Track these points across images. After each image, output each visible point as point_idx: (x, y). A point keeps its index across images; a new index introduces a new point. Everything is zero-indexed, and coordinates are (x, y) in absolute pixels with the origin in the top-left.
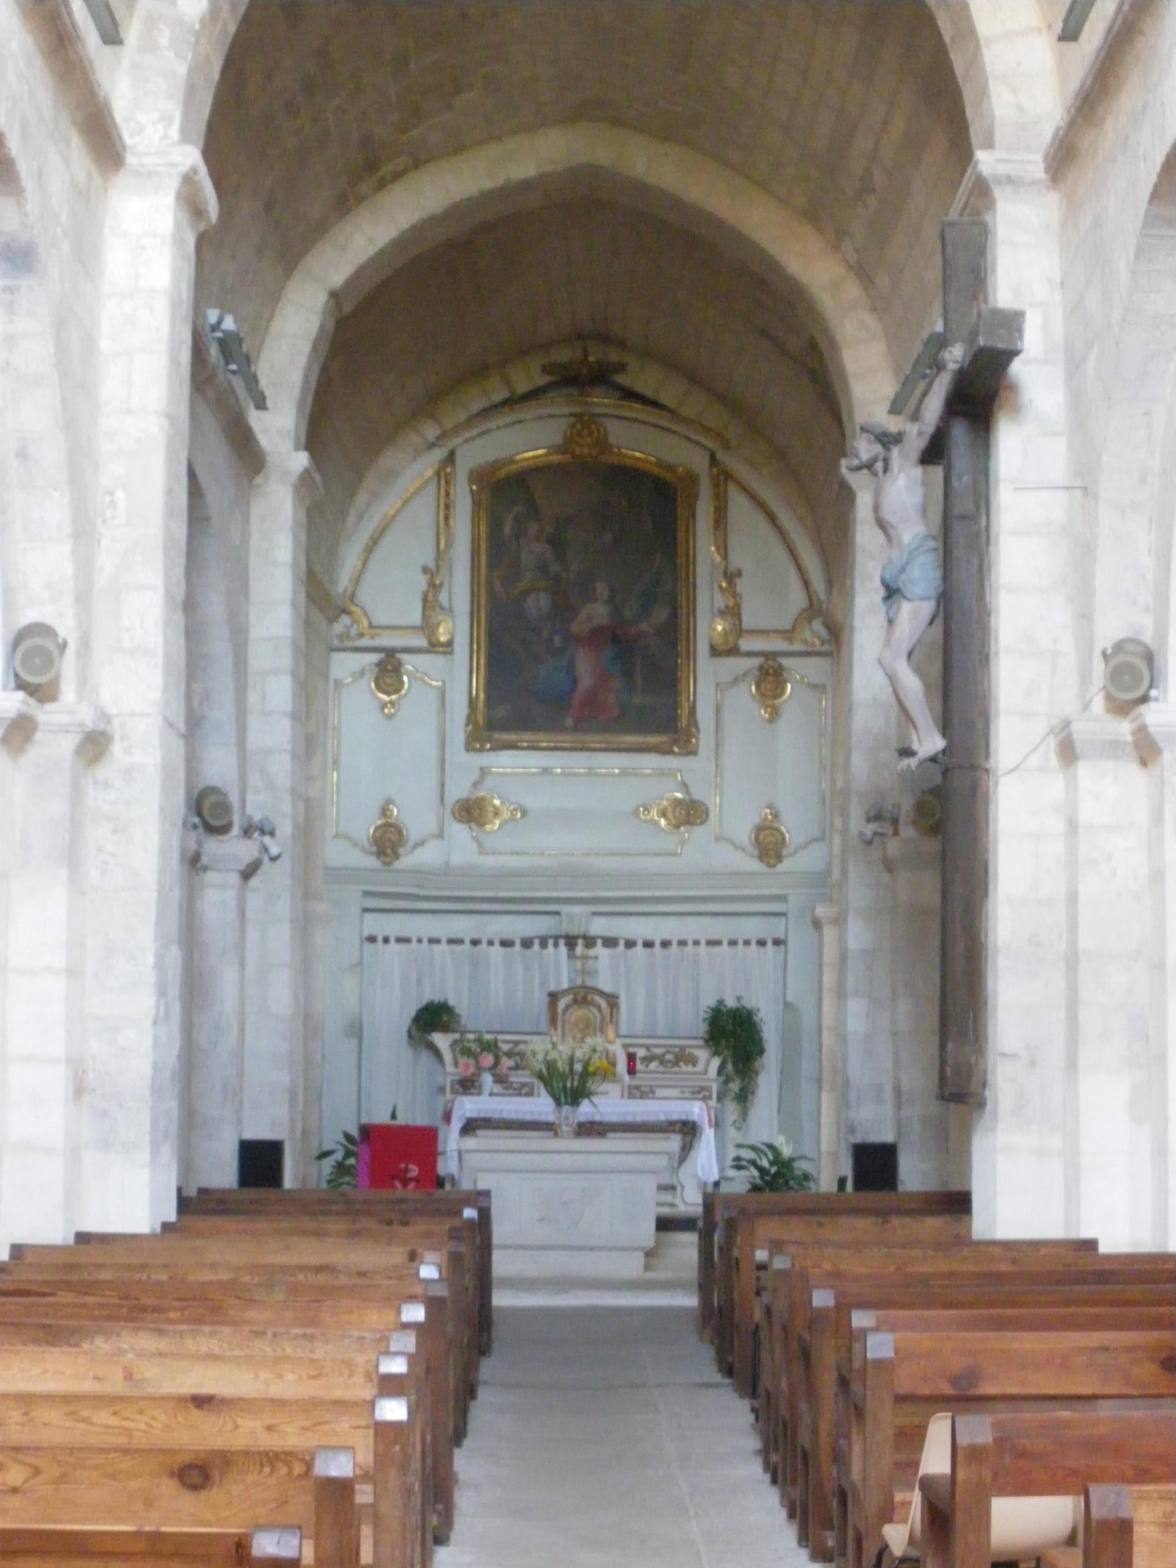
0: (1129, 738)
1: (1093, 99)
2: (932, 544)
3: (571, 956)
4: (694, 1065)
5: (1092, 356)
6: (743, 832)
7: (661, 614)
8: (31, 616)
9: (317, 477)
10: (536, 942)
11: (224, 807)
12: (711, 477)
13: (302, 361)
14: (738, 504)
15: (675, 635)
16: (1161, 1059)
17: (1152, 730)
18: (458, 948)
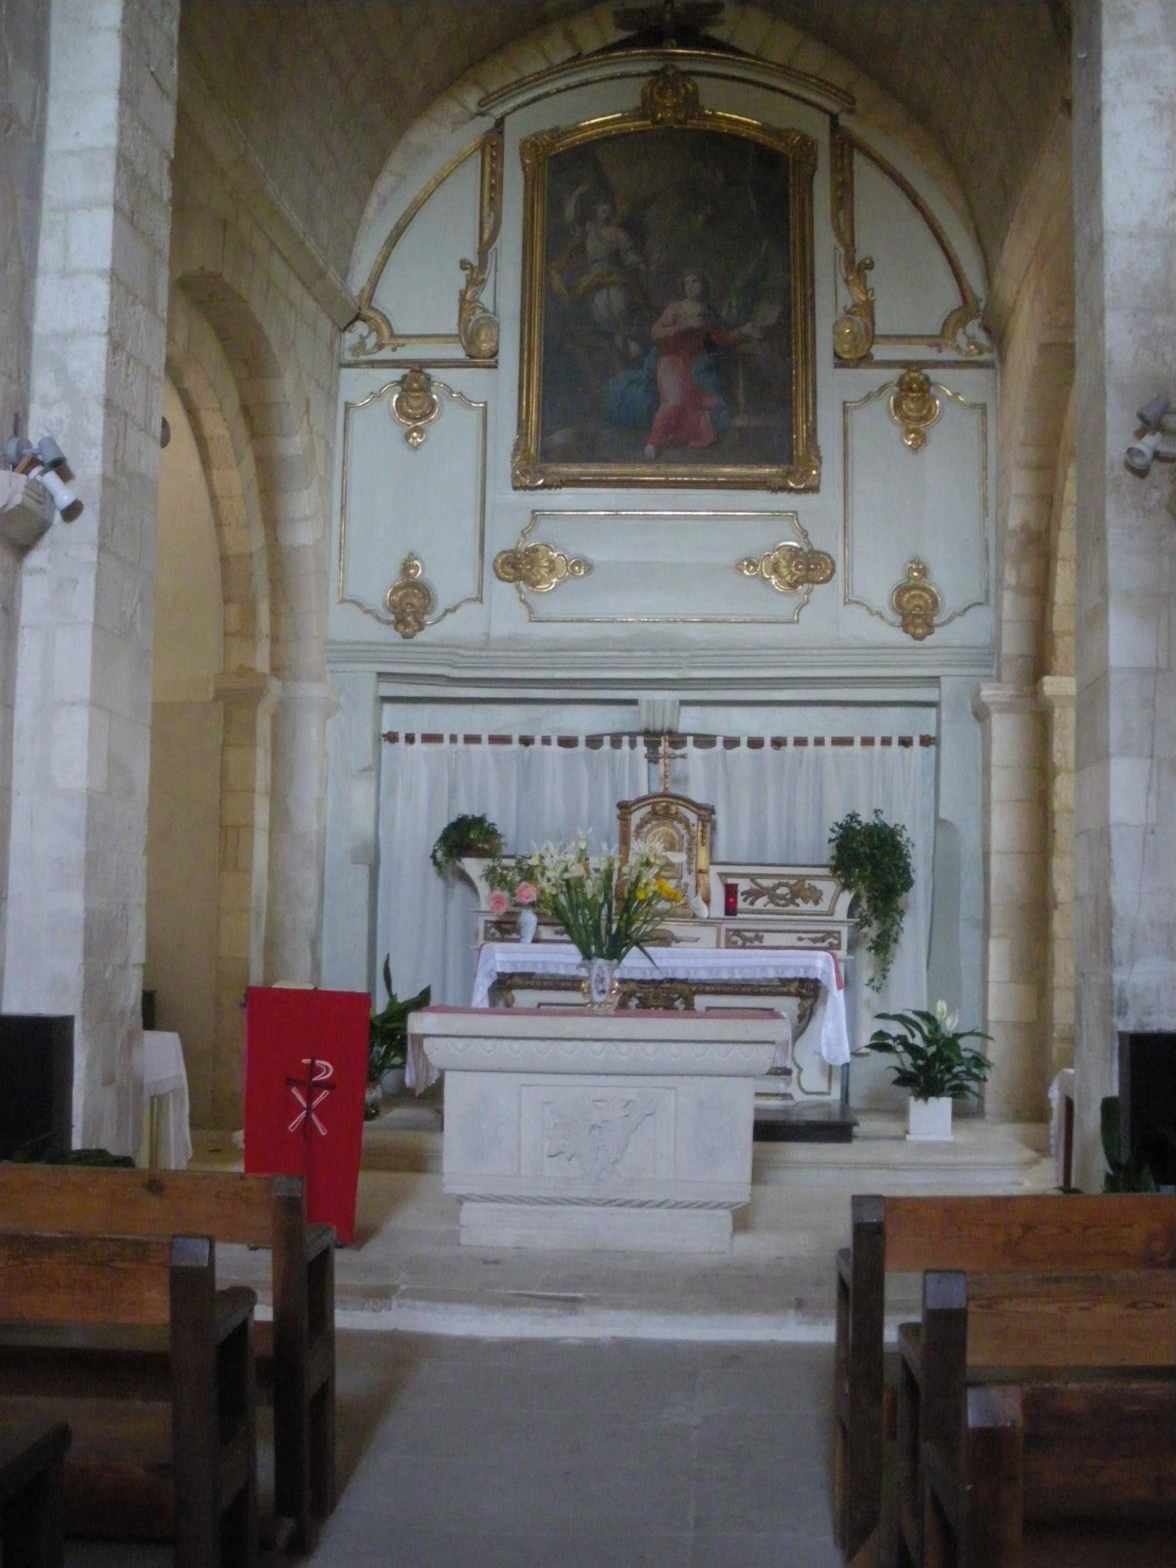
3: (653, 759)
4: (816, 903)
7: (769, 314)
10: (607, 739)
12: (833, 144)
15: (790, 336)
18: (506, 748)
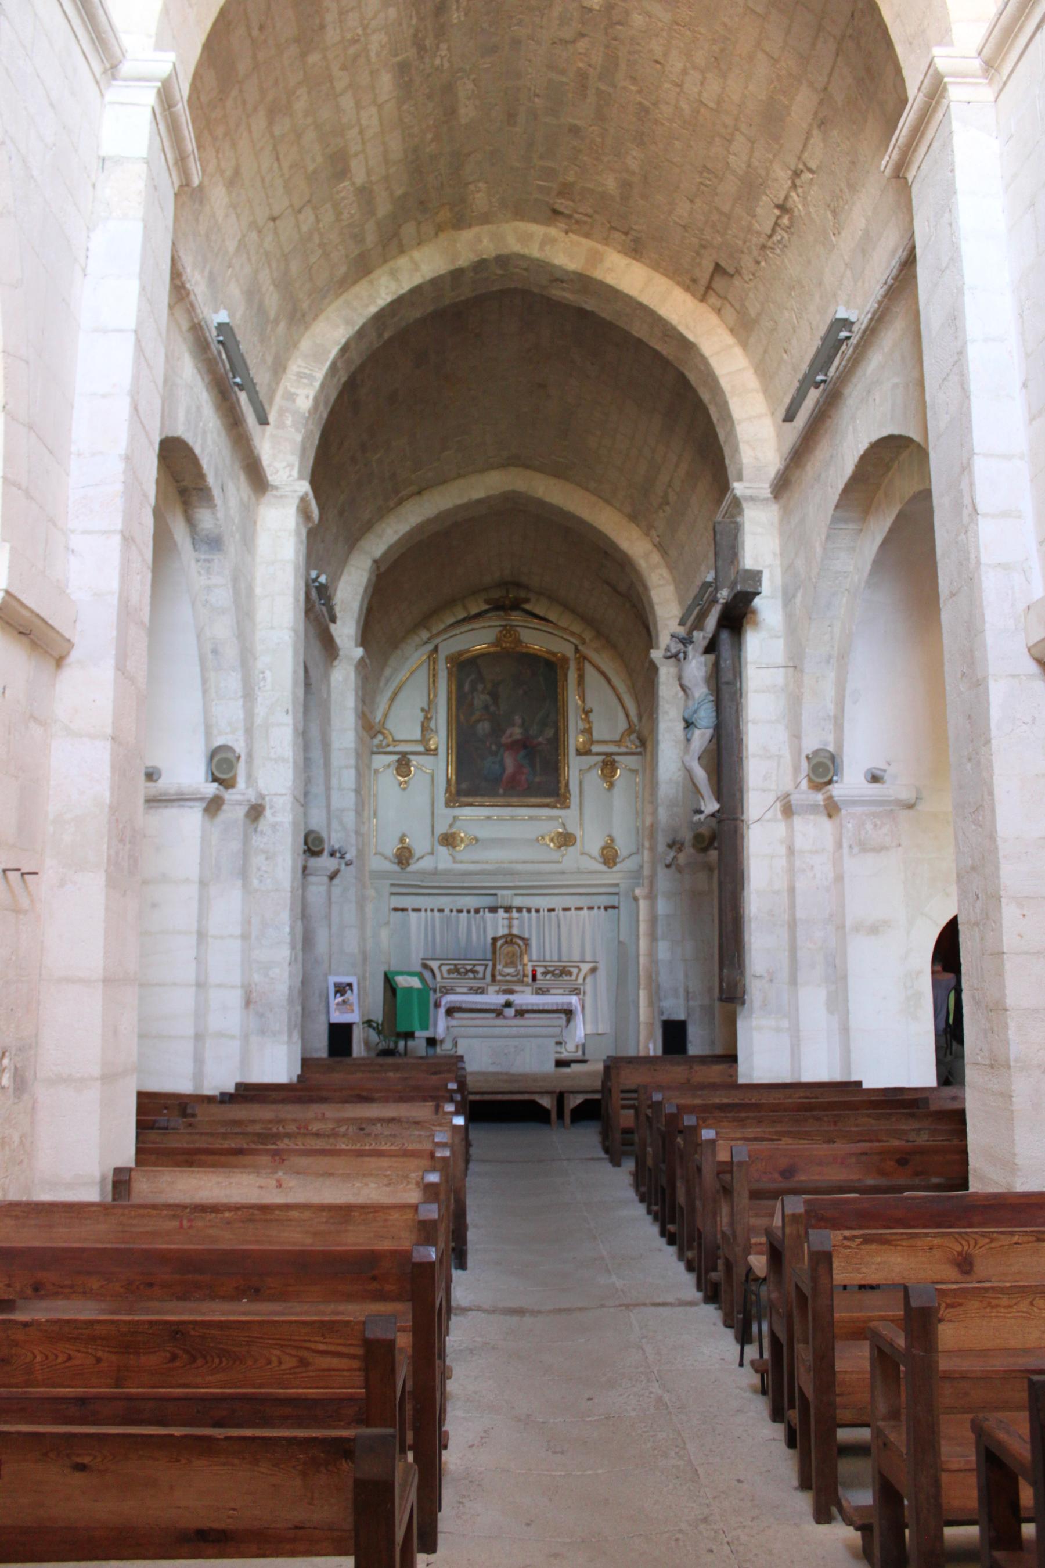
0: (822, 803)
1: (799, 455)
2: (712, 698)
5: (799, 595)
6: (596, 851)
7: (550, 733)
8: (219, 741)
9: (367, 661)
11: (319, 840)
12: (576, 659)
13: (359, 598)
14: (589, 671)
15: (557, 743)
16: (844, 978)
17: (836, 799)
